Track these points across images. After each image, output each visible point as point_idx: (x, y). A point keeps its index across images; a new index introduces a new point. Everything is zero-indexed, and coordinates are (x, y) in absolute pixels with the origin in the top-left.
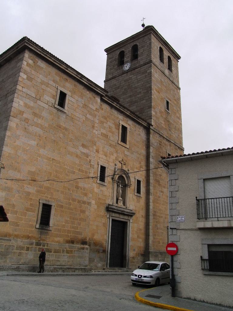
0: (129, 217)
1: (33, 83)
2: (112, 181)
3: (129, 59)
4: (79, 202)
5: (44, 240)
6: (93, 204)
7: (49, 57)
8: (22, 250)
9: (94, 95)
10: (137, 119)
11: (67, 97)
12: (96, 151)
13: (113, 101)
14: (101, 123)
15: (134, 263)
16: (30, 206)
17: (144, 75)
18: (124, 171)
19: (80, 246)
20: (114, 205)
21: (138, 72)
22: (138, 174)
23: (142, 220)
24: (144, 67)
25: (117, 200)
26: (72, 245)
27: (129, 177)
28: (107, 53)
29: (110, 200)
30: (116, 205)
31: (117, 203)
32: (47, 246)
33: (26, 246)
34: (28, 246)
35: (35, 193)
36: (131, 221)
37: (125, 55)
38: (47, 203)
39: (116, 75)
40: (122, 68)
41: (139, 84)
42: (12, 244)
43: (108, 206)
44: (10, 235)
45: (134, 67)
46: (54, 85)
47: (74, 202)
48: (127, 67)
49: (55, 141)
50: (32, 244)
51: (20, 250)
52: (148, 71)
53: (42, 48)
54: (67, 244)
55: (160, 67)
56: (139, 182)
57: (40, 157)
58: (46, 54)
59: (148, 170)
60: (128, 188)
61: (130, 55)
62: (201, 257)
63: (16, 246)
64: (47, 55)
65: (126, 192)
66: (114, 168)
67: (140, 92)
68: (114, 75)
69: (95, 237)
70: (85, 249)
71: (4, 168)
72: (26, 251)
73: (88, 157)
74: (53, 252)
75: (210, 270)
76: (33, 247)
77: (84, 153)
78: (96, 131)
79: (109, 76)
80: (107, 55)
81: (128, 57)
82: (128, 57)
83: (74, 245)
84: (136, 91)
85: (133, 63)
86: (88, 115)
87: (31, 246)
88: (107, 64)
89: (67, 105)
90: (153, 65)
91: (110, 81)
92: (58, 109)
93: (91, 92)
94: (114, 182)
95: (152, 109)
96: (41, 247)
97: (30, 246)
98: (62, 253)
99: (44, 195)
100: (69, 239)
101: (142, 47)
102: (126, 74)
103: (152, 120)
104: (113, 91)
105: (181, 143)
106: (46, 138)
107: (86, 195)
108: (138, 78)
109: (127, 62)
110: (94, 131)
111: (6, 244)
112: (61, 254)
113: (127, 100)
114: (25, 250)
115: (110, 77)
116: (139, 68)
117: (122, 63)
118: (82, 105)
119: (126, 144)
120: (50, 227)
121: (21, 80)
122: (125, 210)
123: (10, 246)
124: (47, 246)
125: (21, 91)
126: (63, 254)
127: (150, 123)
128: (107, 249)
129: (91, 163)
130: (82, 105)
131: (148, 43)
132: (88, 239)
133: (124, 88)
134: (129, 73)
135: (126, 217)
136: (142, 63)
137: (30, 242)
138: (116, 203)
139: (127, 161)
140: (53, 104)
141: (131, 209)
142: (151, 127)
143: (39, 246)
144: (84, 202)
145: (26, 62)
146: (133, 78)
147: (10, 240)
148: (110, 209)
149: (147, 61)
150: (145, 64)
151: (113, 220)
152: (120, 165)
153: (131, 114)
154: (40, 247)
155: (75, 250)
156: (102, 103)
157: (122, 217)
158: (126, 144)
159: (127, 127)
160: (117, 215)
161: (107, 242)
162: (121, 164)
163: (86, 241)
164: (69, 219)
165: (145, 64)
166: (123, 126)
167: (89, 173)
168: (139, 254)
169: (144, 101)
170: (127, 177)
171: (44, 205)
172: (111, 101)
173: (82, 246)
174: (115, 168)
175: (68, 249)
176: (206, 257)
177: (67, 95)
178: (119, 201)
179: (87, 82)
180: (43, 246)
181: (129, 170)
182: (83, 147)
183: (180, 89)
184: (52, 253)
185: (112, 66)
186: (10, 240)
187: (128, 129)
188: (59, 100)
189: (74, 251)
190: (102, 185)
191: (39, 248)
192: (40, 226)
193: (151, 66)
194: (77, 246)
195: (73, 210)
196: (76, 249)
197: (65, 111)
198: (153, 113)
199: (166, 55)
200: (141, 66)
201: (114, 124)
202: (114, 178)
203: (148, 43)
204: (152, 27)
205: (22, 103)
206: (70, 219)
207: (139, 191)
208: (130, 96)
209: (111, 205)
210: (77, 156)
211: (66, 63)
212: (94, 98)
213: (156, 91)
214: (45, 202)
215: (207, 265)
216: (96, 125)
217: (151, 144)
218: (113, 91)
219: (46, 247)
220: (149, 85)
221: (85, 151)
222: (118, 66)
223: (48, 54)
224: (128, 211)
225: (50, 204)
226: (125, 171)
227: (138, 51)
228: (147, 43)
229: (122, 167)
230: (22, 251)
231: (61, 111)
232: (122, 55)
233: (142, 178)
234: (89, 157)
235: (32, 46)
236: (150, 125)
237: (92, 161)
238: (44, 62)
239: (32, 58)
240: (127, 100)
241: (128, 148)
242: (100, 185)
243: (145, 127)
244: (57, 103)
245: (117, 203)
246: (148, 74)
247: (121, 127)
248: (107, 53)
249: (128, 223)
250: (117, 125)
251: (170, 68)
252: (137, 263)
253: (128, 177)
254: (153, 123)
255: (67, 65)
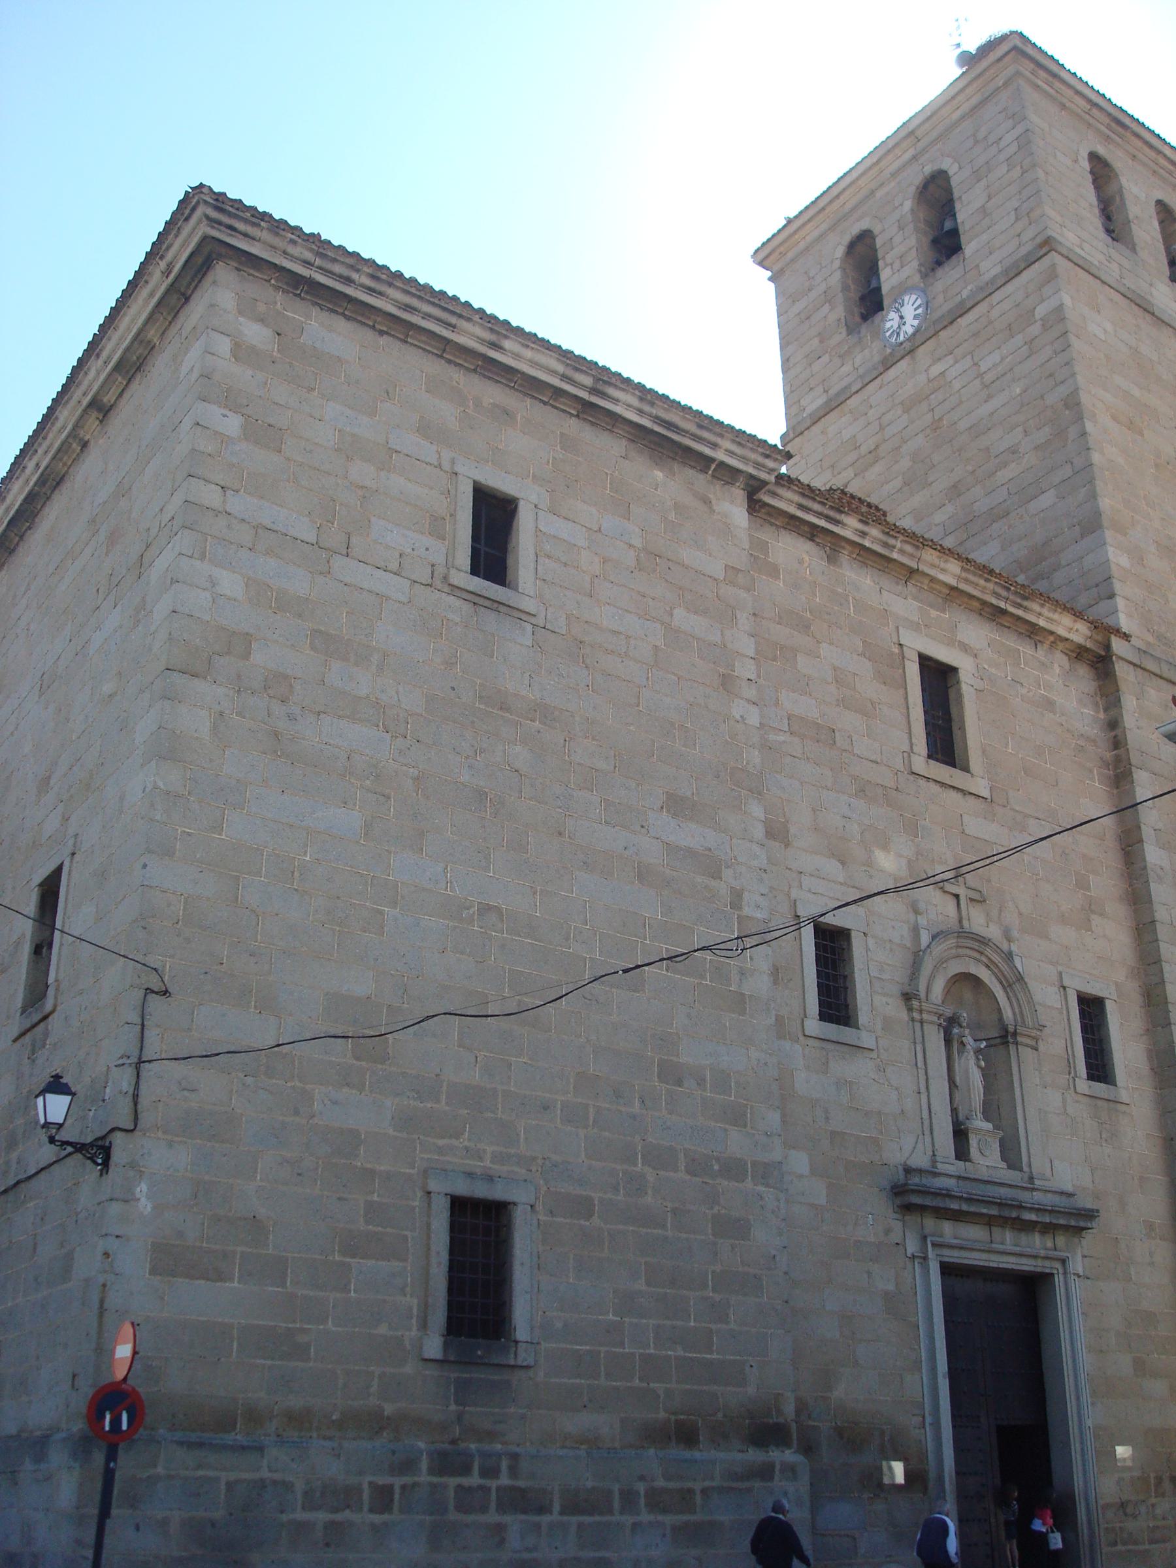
0: (1061, 1240)
1: (288, 459)
2: (904, 1015)
3: (911, 269)
4: (697, 1166)
5: (491, 1436)
6: (801, 1176)
7: (371, 290)
8: (348, 1507)
9: (701, 481)
10: (1019, 606)
11: (525, 524)
12: (770, 834)
13: (832, 513)
14: (774, 659)
15: (1136, 1543)
16: (367, 1223)
17: (1019, 339)
18: (975, 945)
19: (740, 1456)
20: (941, 1167)
21: (976, 335)
22: (1025, 857)
23: (1151, 1254)
24: (1009, 288)
25: (960, 1134)
26: (687, 1454)
27: (1020, 979)
28: (769, 274)
29: (908, 1141)
30: (959, 1167)
31: (962, 1153)
32: (514, 1471)
33: (370, 1483)
34: (382, 1480)
35: (391, 1131)
36: (1077, 1265)
37: (880, 255)
38: (481, 1191)
39: (844, 384)
40: (878, 333)
42: (277, 1476)
43: (902, 1181)
44: (255, 1417)
45: (946, 307)
46: (428, 451)
47: (662, 1173)
49: (481, 795)
50: (407, 1465)
51: (336, 1510)
53: (315, 237)
54: (652, 1451)
55: (1112, 273)
57: (394, 904)
58: (345, 272)
60: (1026, 1053)
61: (912, 241)
63: (300, 1487)
64: (355, 276)
65: (1016, 1084)
66: (905, 931)
67: (1013, 451)
68: (832, 392)
69: (839, 1393)
70: (776, 1478)
71: (166, 993)
72: (371, 1511)
73: (717, 876)
74: (557, 1507)
76: (415, 1485)
77: (690, 852)
78: (754, 710)
79: (803, 403)
80: (772, 286)
83: (697, 1455)
84: (988, 449)
85: (939, 286)
86: (679, 613)
87: (407, 1480)
88: (782, 338)
89: (532, 565)
91: (816, 429)
92: (476, 599)
93: (676, 467)
94: (922, 1022)
95: (1109, 535)
96: (474, 1480)
97: (398, 1482)
98: (621, 1513)
99: (455, 1142)
100: (662, 1415)
101: (977, 176)
102: (903, 365)
103: (1120, 603)
106: (417, 779)
107: (737, 1117)
108: (983, 369)
109: (903, 289)
110: (738, 709)
111: (233, 1476)
112: (616, 1518)
114: (366, 1507)
116: (981, 309)
118: (632, 553)
119: (966, 769)
120: (522, 1348)
121: (210, 449)
122: (1025, 1196)
123: (262, 1484)
124: (514, 1471)
125: (217, 513)
126: (628, 1520)
127: (1110, 621)
128: (931, 1457)
129: (747, 911)
130: (632, 553)
131: (1009, 138)
132: (789, 1409)
134: (921, 350)
135: (1037, 1242)
136: (997, 270)
137: (394, 1452)
138: (958, 1157)
139: (989, 881)
140: (440, 571)
141: (1069, 1188)
142: (1117, 645)
143: (460, 1475)
144: (734, 1169)
145: (227, 340)
147: (260, 1449)
148: (916, 1200)
149: (1024, 251)
150: (1013, 273)
151: (947, 1270)
152: (950, 907)
153: (966, 580)
154: (465, 1481)
155: (707, 1483)
156: (766, 534)
157: (1008, 1238)
158: (966, 769)
159: (954, 663)
160: (974, 1233)
161: (928, 1420)
162: (952, 902)
163: (781, 1420)
164: (641, 1285)
165: (1013, 273)
166: (926, 662)
167: (742, 973)
168: (1159, 1480)
169: (1047, 499)
170: (1007, 986)
171: (460, 1206)
172: (819, 514)
173: (754, 1456)
174: (915, 930)
175: (660, 1483)
177: (522, 506)
178: (973, 1141)
179: (641, 412)
180: (487, 1472)
181: (1015, 934)
182: (675, 815)
184: (555, 1517)
185: (816, 341)
186: (260, 1449)
188: (475, 538)
189: (704, 1491)
190: (845, 1048)
191: (459, 1487)
192: (446, 1346)
194: (722, 1455)
195: (664, 1227)
196: (712, 1479)
197: (529, 605)
198: (1118, 559)
199: (1143, 196)
200: (988, 291)
201: (863, 654)
202: (917, 997)
204: (1018, 43)
205: (230, 584)
206: (648, 1284)
208: (956, 490)
209: (920, 1171)
210: (643, 874)
211: (481, 311)
212: (707, 502)
213: (1114, 418)
214: (463, 1188)
216: (745, 669)
217: (1135, 758)
219: (505, 1480)
220: (1063, 391)
221: (692, 835)
222: (850, 331)
223: (358, 271)
224: (1048, 1200)
225: (497, 1193)
226: (983, 941)
227: (958, 206)
228: (1003, 144)
229: (960, 921)
230: (347, 1515)
231: (497, 605)
234: (727, 873)
235: (245, 235)
236: (1106, 630)
237: (746, 895)
238: (341, 324)
239: (261, 308)
241: (985, 793)
242: (824, 1044)
243: (1079, 653)
244: (464, 558)
245: (962, 1153)
246: (1045, 328)
247: (913, 670)
248: (769, 274)
249: (1059, 1281)
252: (1151, 1542)
253: (1014, 982)
254: (1125, 622)
255: (493, 318)
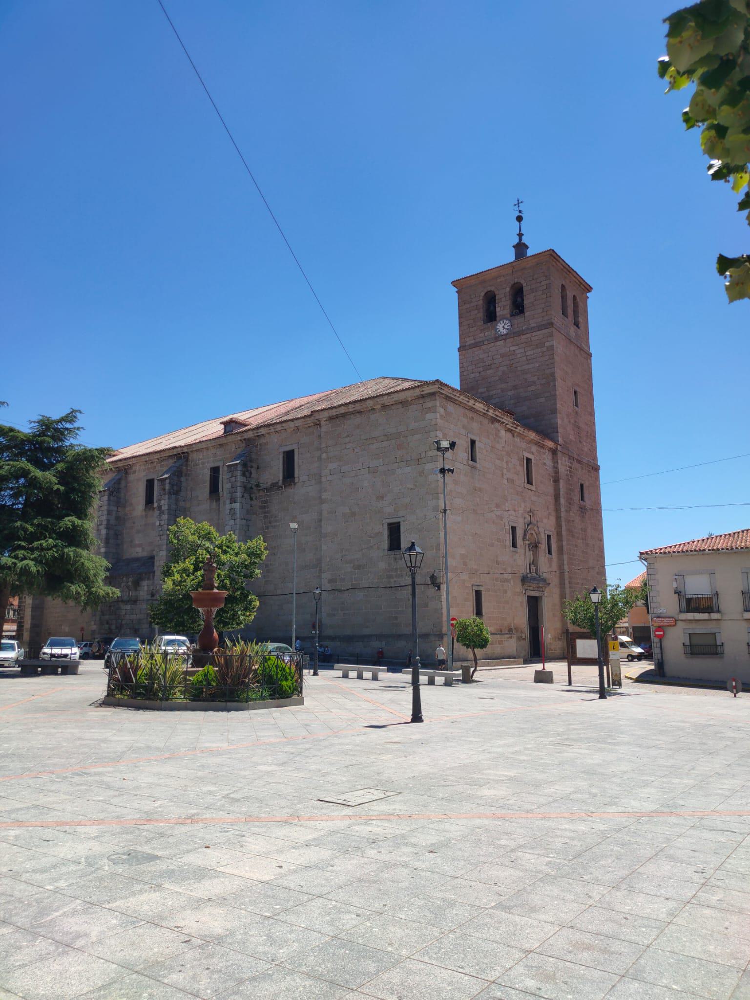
28: (457, 290)
41: (531, 366)
48: (502, 327)
52: (547, 344)
56: (549, 537)
59: (558, 518)
62: (684, 644)
75: (692, 654)
81: (503, 307)
82: (503, 307)
90: (554, 330)
104: (480, 373)
105: (595, 458)
113: (510, 393)
115: (470, 341)
117: (491, 317)
133: (501, 369)
146: (517, 352)
149: (544, 323)
165: (540, 328)
176: (688, 643)
183: (590, 355)
187: (533, 461)
193: (551, 335)
198: (559, 421)
203: (543, 283)
207: (550, 553)
208: (515, 387)
215: (688, 649)
218: (480, 373)
232: (491, 300)
233: (552, 532)
240: (510, 393)
248: (457, 290)
250: (521, 460)
251: (576, 324)
